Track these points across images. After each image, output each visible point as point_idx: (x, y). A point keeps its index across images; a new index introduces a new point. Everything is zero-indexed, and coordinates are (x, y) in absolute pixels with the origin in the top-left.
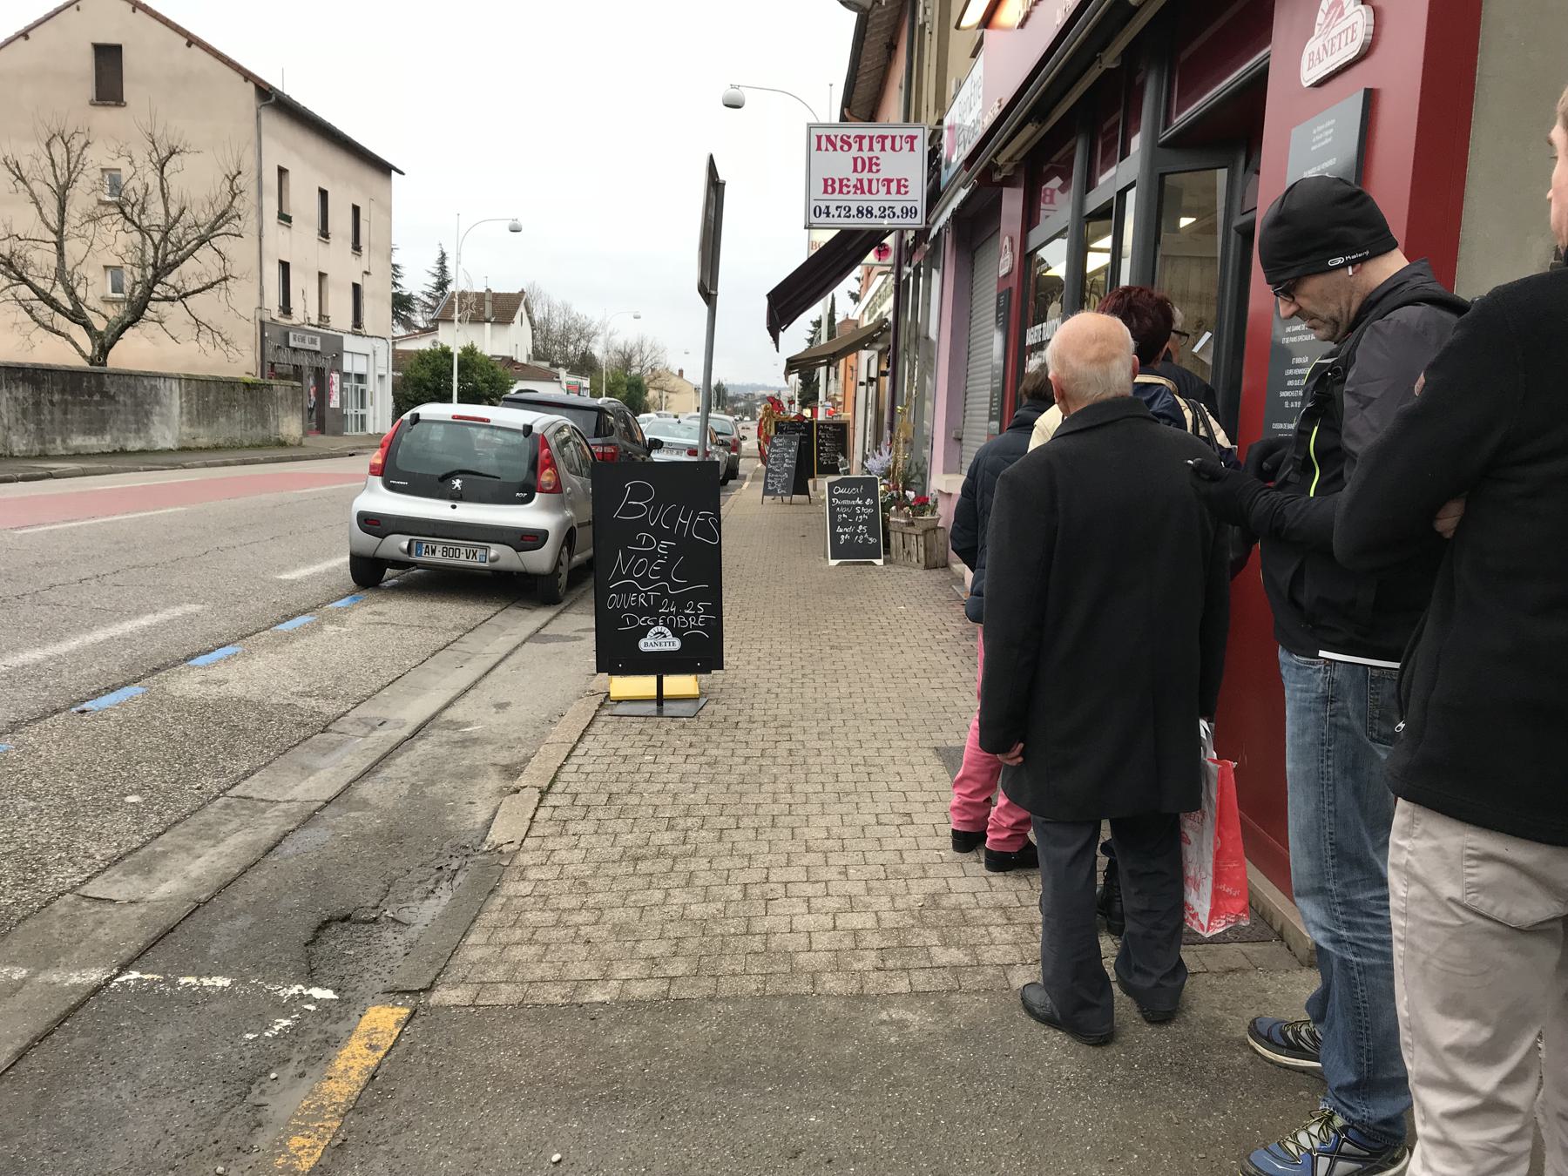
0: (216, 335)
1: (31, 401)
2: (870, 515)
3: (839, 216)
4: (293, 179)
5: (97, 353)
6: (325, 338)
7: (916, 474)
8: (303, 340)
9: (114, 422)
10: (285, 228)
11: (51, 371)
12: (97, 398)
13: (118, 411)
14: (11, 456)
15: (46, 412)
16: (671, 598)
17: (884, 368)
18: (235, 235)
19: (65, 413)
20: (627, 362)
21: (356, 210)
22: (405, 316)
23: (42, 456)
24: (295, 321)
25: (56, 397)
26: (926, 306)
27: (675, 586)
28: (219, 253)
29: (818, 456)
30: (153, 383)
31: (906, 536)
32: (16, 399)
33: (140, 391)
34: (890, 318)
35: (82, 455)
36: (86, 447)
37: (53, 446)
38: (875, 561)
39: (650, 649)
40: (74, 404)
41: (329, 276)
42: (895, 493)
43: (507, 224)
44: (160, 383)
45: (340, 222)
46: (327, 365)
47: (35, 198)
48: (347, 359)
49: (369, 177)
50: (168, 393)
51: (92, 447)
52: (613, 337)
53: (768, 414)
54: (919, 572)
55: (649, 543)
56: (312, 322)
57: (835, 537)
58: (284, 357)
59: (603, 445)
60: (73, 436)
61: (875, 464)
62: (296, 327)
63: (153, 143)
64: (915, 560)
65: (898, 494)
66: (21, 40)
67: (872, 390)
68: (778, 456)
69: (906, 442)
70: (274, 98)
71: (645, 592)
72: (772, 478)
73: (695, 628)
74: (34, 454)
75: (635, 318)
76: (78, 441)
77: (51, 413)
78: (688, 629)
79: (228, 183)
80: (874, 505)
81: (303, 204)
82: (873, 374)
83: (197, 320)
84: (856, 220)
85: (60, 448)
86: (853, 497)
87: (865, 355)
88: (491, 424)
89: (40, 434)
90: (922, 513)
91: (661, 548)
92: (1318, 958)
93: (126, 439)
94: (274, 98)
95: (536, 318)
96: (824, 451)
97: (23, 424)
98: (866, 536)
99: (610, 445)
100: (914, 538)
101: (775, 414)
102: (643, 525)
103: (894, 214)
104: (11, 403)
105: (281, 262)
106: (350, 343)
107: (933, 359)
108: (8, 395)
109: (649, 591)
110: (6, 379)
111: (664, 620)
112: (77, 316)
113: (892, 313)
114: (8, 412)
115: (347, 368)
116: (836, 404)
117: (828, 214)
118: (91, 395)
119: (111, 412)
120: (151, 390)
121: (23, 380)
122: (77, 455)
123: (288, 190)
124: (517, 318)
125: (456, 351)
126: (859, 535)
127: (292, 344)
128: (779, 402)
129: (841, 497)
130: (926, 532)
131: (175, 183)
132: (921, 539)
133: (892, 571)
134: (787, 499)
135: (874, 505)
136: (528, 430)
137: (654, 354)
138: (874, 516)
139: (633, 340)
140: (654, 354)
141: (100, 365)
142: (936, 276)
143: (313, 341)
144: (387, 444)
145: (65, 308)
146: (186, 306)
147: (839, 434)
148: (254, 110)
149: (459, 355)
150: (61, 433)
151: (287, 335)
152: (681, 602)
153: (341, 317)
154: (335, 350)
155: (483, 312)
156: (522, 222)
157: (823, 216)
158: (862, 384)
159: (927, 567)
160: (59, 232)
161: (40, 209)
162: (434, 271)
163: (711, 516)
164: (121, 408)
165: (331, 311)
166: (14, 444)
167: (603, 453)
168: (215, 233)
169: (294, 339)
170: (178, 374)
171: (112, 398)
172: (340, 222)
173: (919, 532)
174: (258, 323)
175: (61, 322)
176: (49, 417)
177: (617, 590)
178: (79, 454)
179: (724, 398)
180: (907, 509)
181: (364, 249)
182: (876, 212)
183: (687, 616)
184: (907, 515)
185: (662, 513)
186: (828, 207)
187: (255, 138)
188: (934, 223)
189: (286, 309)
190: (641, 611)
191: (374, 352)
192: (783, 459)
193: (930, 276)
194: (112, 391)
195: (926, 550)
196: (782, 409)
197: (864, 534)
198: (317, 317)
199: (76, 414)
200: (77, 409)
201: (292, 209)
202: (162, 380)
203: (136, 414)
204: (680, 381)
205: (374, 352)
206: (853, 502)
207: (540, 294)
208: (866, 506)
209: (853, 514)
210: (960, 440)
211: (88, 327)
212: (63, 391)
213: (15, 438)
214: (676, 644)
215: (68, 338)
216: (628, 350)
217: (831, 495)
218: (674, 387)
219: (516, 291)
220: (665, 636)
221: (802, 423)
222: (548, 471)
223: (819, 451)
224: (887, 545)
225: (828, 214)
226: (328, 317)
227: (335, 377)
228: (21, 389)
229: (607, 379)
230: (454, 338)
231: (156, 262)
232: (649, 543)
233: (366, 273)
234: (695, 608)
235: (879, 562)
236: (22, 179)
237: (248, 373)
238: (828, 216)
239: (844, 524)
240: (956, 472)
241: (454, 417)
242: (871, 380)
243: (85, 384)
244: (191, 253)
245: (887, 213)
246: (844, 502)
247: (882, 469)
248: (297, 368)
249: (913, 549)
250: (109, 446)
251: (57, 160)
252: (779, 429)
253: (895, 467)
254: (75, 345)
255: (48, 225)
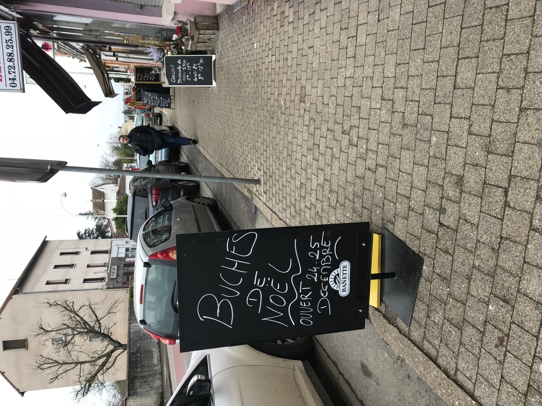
0: (113, 307)
1: (141, 380)
2: (187, 62)
3: (14, 72)
4: (50, 279)
5: (122, 348)
6: (112, 265)
7: (162, 34)
8: (113, 272)
9: (148, 347)
10: (70, 281)
11: (129, 373)
12: (139, 355)
13: (144, 346)
14: (162, 386)
15: (145, 374)
16: (305, 272)
17: (107, 49)
18: (73, 304)
19: (145, 366)
20: (116, 149)
21: (62, 254)
22: (104, 227)
23: (162, 373)
24: (106, 276)
25: (139, 370)
26: (70, 24)
27: (295, 269)
28: (81, 308)
29: (151, 81)
30: (132, 334)
31: (200, 40)
32: (141, 386)
33: (136, 338)
34: (81, 44)
35: (161, 359)
36: (157, 358)
37: (157, 370)
38: (213, 60)
39: (348, 287)
40: (142, 363)
41: (89, 263)
42: (172, 46)
43: (63, 198)
44: (132, 331)
45: (67, 260)
46: (123, 263)
47: (64, 372)
48: (120, 256)
49: (48, 249)
50: (136, 328)
51: (157, 355)
52: (107, 153)
53: (133, 104)
54: (221, 34)
55: (255, 295)
56: (106, 270)
57: (199, 82)
58: (120, 279)
59: (152, 195)
60: (154, 362)
61: (155, 55)
62: (109, 275)
63: (38, 335)
64: (213, 36)
65: (172, 44)
66: (4, 374)
67: (119, 54)
68: (152, 101)
69: (144, 39)
70: (18, 288)
71: (299, 294)
72: (163, 104)
73: (332, 250)
74: (161, 377)
75: (99, 146)
76: (155, 361)
77: (145, 372)
78: (333, 255)
79: (53, 306)
80: (182, 59)
81: (60, 274)
82: (112, 54)
83: (108, 314)
84: (16, 62)
85: (158, 367)
86: (177, 71)
87: (103, 57)
88: (144, 285)
89: (154, 375)
90: (186, 30)
91: (261, 284)
92: (157, 30)
93: (154, 342)
94: (18, 288)
95: (101, 183)
96: (149, 78)
97: (150, 382)
98: (199, 64)
99: (151, 191)
100: (201, 36)
101: (133, 101)
102: (239, 302)
103: (10, 40)
104: (142, 387)
105: (84, 282)
106: (114, 255)
107: (102, 21)
108: (139, 389)
109: (298, 291)
110: (133, 390)
111: (324, 276)
112: (109, 355)
113: (79, 44)
114: (145, 388)
115: (123, 255)
116: (129, 68)
117: (14, 79)
118: (138, 357)
119: (144, 349)
120: (135, 334)
121: (133, 383)
122: (161, 360)
123: (55, 281)
124: (102, 190)
125: (115, 215)
126: (198, 68)
127: (115, 277)
128: (127, 99)
129: (177, 78)
130: (198, 29)
131: (53, 326)
132: (201, 32)
133: (220, 50)
134: (172, 98)
135: (182, 59)
136: (147, 265)
137: (113, 138)
138: (188, 60)
139: (108, 146)
140: (113, 138)
141: (126, 346)
142: (58, 18)
143: (114, 269)
144: (158, 337)
145: (106, 359)
146: (103, 318)
147: (140, 71)
148: (23, 295)
149: (117, 215)
150: (153, 367)
151: (112, 279)
152: (309, 263)
153: (104, 259)
154: (117, 261)
155: (100, 202)
156: (62, 193)
157: (15, 82)
158: (117, 59)
159: (218, 29)
160: (77, 363)
161: (68, 370)
162: (86, 217)
163: (230, 240)
164: (142, 345)
165: (101, 262)
166: (158, 385)
167: (155, 195)
168: (73, 310)
169: (113, 276)
170: (128, 324)
171: (139, 349)
172: (67, 260)
173: (197, 33)
174: (107, 290)
175: (111, 360)
176: (147, 372)
177: (296, 318)
178: (160, 360)
179: (128, 111)
180: (183, 40)
181: (77, 250)
182: (10, 51)
183: (321, 256)
184: (187, 40)
185: (228, 285)
186: (10, 79)
187: (34, 294)
188: (13, 16)
189: (102, 279)
190: (315, 297)
191: (117, 245)
192: (154, 99)
193: (59, 21)
194: (136, 349)
195: (208, 29)
196: (130, 98)
197: (198, 66)
198: (104, 267)
199: (145, 362)
200: (143, 362)
201: (63, 279)
202: (131, 330)
203: (144, 340)
204: (122, 128)
205: (117, 245)
206: (180, 71)
207: (92, 182)
208: (182, 64)
209: (187, 72)
210: (142, 6)
211: (112, 351)
212: (137, 368)
213: (155, 385)
214: (346, 264)
215: (117, 357)
216: (112, 148)
217: (176, 84)
218: (125, 131)
219: (91, 190)
220: (338, 275)
221: (136, 89)
222: (170, 254)
223: (149, 81)
224: (205, 52)
225: (14, 79)
226: (104, 263)
227: (127, 260)
228: (136, 384)
229: (123, 157)
230: (111, 215)
231: (86, 332)
232: (255, 295)
233: (86, 249)
234: (315, 250)
235: (214, 57)
236: (57, 377)
237: (127, 293)
238: (15, 79)
239: (192, 77)
240: (161, 9)
241: (141, 303)
242: (114, 55)
243: (134, 360)
244: (82, 318)
245: (10, 44)
246: (180, 76)
247: (158, 52)
248: (124, 274)
249: (207, 37)
250: (157, 349)
251: (48, 366)
252: (139, 99)
253: (157, 46)
254: (119, 355)
255: (74, 367)
